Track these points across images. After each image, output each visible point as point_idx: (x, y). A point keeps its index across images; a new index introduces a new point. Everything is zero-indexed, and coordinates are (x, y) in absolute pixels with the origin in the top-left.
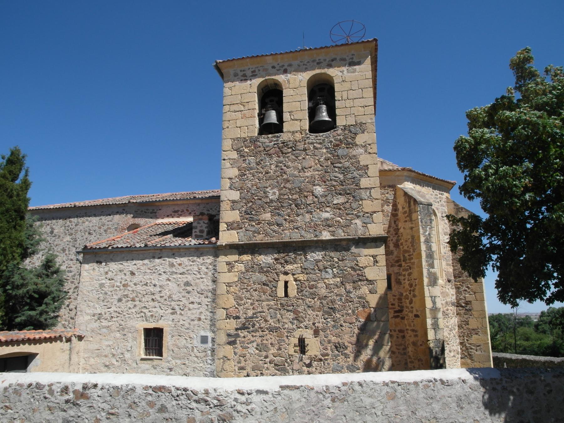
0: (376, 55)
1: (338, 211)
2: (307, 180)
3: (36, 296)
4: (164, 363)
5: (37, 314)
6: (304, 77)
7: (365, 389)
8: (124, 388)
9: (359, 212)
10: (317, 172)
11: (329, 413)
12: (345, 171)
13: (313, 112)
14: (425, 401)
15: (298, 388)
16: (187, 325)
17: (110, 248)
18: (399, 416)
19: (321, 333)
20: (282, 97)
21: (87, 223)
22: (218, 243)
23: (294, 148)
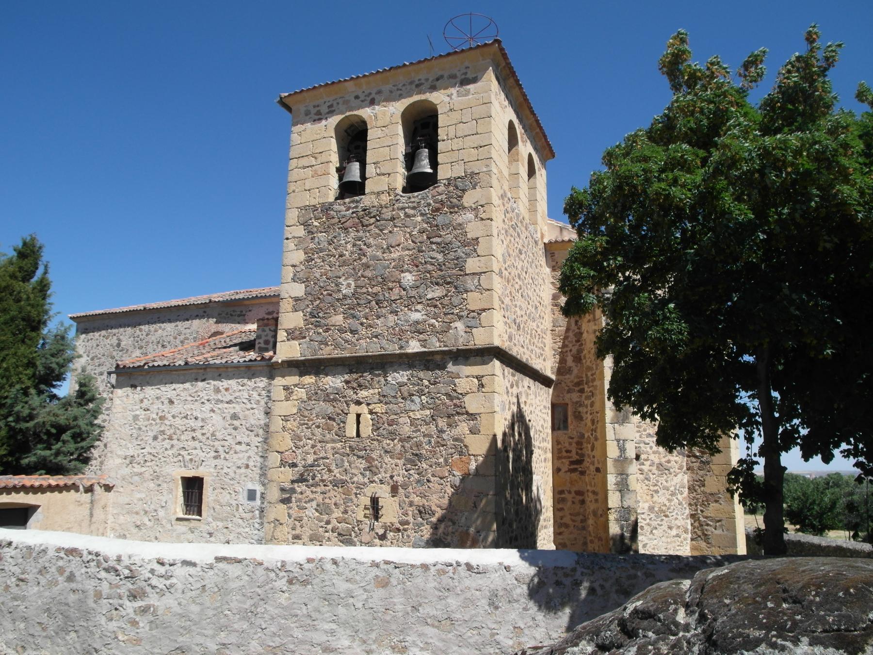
0: (508, 64)
1: (433, 309)
2: (393, 264)
3: (54, 431)
4: (203, 526)
5: (52, 455)
6: (397, 108)
7: (341, 569)
8: (36, 549)
9: (462, 310)
10: (407, 252)
11: (283, 599)
12: (445, 248)
13: (410, 159)
14: (437, 593)
15: (239, 561)
16: (232, 475)
17: (146, 367)
18: (391, 612)
19: (401, 490)
20: (366, 141)
21: (160, 331)
22: (274, 360)
23: (378, 217)
